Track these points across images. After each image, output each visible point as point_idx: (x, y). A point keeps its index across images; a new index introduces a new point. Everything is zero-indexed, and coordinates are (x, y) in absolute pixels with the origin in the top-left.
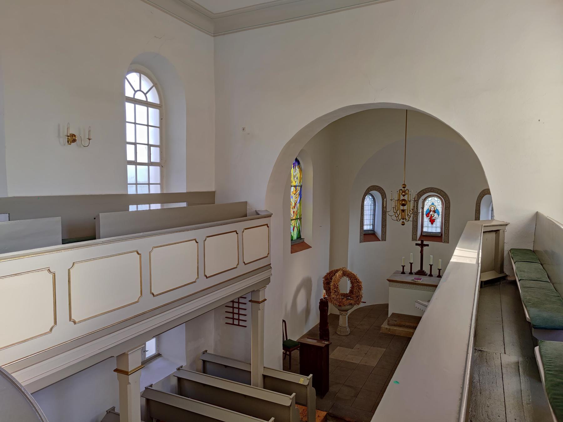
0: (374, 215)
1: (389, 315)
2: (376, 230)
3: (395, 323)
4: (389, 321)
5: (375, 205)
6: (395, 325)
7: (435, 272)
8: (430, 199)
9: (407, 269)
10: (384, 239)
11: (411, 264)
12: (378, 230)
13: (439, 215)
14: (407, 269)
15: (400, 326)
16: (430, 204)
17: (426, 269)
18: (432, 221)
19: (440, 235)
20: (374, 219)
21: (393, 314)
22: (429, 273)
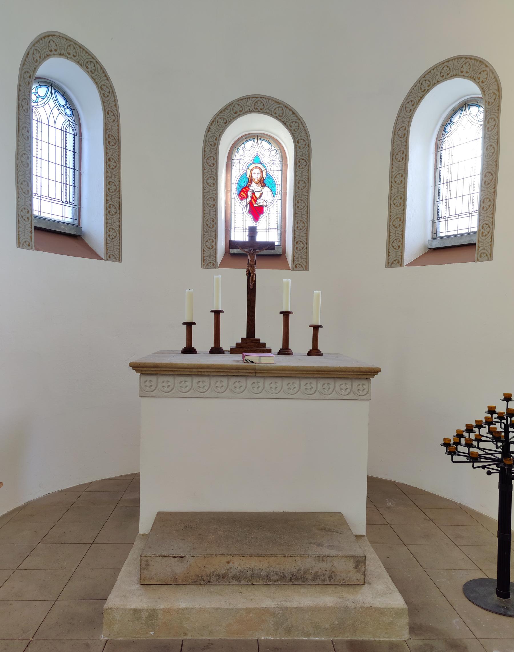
0: (78, 170)
1: (146, 521)
2: (85, 224)
3: (180, 569)
4: (145, 565)
5: (79, 134)
6: (176, 582)
7: (301, 342)
8: (249, 144)
9: (203, 340)
10: (113, 252)
11: (217, 313)
12: (94, 225)
13: (274, 193)
14: (203, 340)
15: (203, 580)
16: (248, 159)
17: (269, 332)
18: (256, 212)
19: (278, 251)
20: (78, 186)
21: (163, 519)
22: (276, 345)
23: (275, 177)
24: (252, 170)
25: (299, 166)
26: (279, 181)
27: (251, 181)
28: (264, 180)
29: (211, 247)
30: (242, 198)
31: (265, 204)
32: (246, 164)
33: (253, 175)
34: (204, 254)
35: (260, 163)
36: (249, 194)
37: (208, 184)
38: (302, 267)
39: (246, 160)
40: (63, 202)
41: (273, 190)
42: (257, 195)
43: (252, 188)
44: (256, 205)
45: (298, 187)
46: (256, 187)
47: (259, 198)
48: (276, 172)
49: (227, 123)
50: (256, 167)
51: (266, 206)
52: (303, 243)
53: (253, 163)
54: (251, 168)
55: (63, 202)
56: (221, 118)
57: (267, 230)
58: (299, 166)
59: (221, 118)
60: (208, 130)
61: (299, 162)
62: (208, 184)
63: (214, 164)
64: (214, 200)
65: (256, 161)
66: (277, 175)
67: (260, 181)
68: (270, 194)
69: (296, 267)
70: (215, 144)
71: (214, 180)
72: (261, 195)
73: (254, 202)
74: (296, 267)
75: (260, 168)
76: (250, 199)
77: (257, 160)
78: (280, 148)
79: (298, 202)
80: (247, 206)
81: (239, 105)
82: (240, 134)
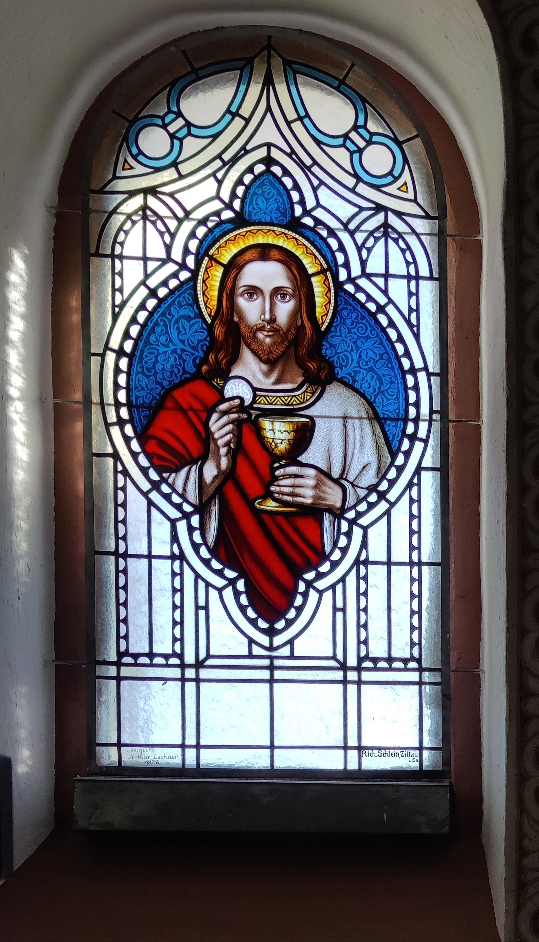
13: (391, 428)
16: (202, 195)
24: (233, 268)
26: (424, 348)
27: (228, 336)
28: (320, 336)
31: (333, 496)
32: (187, 227)
33: (242, 302)
35: (294, 225)
36: (220, 428)
39: (189, 199)
40: (343, 667)
42: (278, 433)
44: (271, 505)
46: (267, 383)
48: (398, 290)
51: (338, 514)
53: (241, 221)
55: (343, 667)
65: (262, 207)
66: (399, 282)
72: (303, 436)
73: (252, 486)
75: (289, 260)
76: (224, 463)
77: (267, 203)
78: (422, 133)
80: (202, 509)
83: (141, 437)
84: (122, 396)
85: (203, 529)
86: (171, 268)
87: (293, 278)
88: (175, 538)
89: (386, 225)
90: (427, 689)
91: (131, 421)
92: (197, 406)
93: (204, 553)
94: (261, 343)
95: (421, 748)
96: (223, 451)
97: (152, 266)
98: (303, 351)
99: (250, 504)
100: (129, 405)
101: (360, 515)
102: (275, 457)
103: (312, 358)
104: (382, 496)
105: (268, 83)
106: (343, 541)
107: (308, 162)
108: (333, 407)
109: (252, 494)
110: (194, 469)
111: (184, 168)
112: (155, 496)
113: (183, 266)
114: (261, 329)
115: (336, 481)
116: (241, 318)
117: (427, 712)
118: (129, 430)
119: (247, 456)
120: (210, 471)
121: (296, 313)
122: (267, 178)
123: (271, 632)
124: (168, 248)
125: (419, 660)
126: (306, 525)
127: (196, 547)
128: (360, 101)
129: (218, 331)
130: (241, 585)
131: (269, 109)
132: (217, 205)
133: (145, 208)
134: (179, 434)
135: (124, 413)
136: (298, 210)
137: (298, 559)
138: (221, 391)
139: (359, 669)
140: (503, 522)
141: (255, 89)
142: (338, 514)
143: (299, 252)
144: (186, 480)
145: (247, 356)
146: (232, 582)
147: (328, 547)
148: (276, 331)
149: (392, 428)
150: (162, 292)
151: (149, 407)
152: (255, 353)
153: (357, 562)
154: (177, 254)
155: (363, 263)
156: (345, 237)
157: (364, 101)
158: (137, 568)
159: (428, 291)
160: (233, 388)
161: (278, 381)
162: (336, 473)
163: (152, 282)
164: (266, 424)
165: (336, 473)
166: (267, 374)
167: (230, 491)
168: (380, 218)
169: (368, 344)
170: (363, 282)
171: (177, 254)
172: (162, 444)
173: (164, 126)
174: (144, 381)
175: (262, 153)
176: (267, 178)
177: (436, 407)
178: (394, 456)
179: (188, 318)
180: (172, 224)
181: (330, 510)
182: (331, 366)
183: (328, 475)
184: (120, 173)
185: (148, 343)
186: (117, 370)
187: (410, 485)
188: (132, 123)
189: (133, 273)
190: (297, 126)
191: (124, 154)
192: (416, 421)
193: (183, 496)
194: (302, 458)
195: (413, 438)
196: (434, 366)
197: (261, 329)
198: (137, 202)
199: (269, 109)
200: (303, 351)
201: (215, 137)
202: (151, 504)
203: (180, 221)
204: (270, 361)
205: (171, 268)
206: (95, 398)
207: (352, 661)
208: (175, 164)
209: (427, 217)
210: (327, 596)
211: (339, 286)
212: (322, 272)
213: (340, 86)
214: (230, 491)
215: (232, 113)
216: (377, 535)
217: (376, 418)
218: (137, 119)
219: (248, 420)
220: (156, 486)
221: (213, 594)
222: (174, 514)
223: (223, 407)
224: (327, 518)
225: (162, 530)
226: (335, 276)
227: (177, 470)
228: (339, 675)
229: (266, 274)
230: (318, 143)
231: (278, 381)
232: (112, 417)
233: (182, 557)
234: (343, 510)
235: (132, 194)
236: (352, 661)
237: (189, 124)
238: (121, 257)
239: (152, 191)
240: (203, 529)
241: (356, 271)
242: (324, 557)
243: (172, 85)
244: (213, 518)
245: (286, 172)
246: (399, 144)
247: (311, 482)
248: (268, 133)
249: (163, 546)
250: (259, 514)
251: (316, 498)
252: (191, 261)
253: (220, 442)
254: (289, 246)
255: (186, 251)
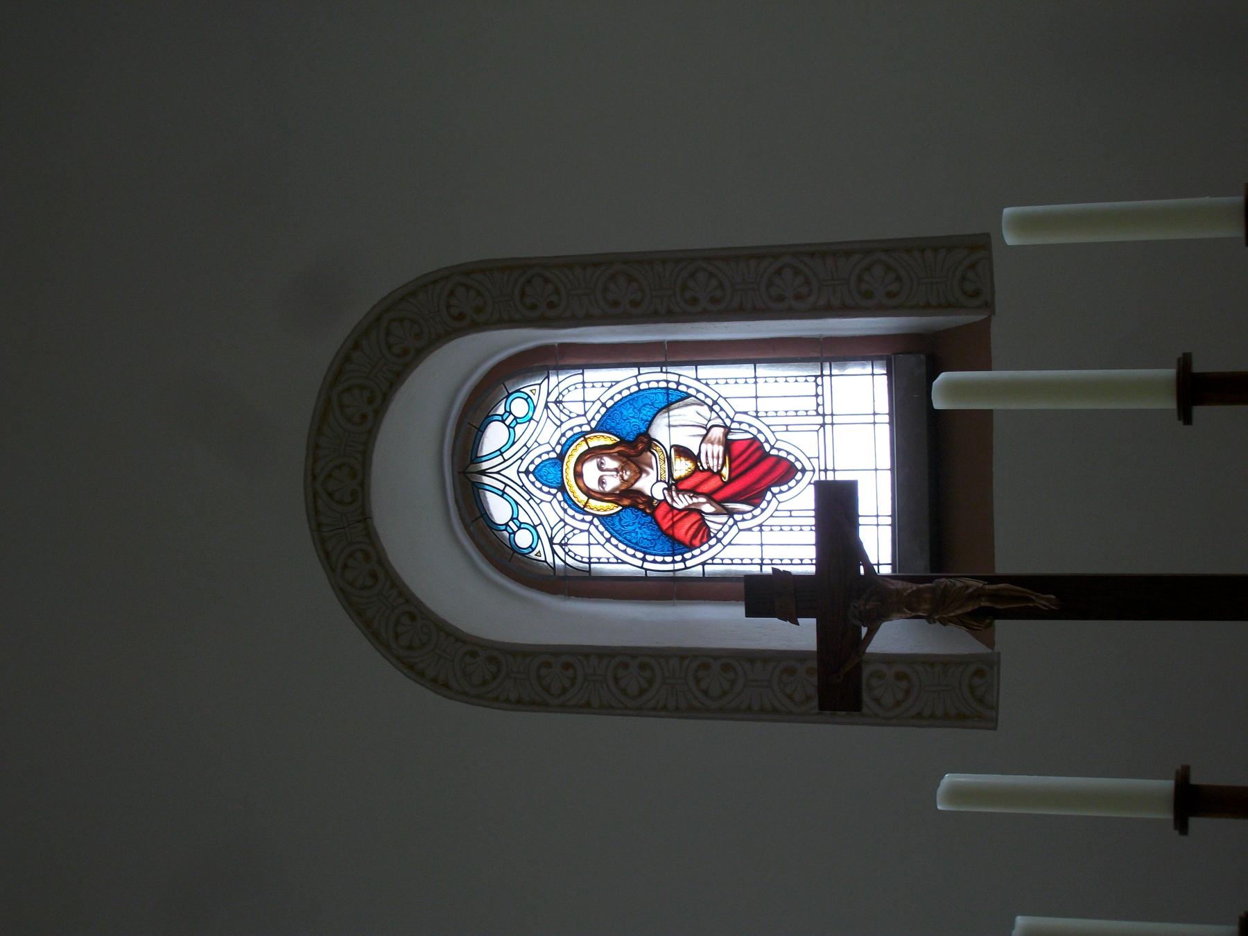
13: (672, 399)
16: (550, 511)
18: (752, 471)
23: (610, 396)
24: (589, 493)
25: (551, 305)
29: (904, 684)
30: (703, 533)
31: (717, 433)
33: (608, 488)
34: (932, 716)
35: (561, 457)
36: (682, 502)
37: (642, 692)
38: (972, 266)
39: (553, 519)
40: (823, 425)
41: (661, 400)
42: (682, 467)
43: (658, 493)
44: (725, 472)
45: (635, 304)
46: (653, 473)
47: (695, 458)
48: (592, 394)
49: (411, 611)
50: (578, 475)
51: (728, 430)
52: (868, 268)
53: (562, 488)
54: (581, 498)
55: (823, 425)
56: (397, 636)
57: (825, 420)
58: (551, 305)
59: (397, 636)
60: (441, 686)
61: (534, 307)
62: (642, 692)
63: (567, 666)
64: (706, 666)
67: (628, 457)
68: (681, 414)
69: (976, 294)
70: (491, 659)
71: (626, 666)
72: (683, 452)
73: (714, 483)
74: (976, 294)
75: (582, 460)
76: (702, 500)
79: (695, 301)
80: (731, 513)
81: (345, 566)
82: (457, 540)
83: (691, 548)
84: (669, 559)
85: (743, 513)
86: (592, 529)
87: (591, 458)
88: (750, 529)
89: (557, 402)
90: (834, 372)
91: (682, 554)
92: (670, 516)
93: (757, 512)
94: (630, 477)
95: (873, 374)
96: (695, 500)
97: (593, 541)
98: (632, 452)
99: (725, 484)
100: (673, 555)
101: (728, 416)
102: (696, 469)
103: (636, 447)
104: (715, 403)
105: (484, 473)
106: (744, 427)
107: (525, 449)
108: (660, 431)
109: (720, 483)
110: (707, 517)
111: (537, 522)
112: (725, 541)
113: (591, 523)
114: (622, 477)
115: (708, 431)
116: (617, 489)
117: (846, 372)
118: (687, 556)
119: (697, 486)
120: (708, 508)
121: (611, 456)
122: (537, 473)
123: (804, 471)
124: (582, 531)
125: (816, 377)
126: (736, 450)
127: (754, 517)
128: (487, 420)
129: (626, 502)
130: (775, 490)
131: (498, 473)
132: (555, 502)
133: (560, 544)
134: (687, 526)
135: (678, 558)
136: (553, 455)
137: (758, 454)
138: (660, 502)
139: (824, 415)
140: (726, 324)
141: (486, 480)
142: (728, 430)
143: (576, 455)
144: (715, 523)
145: (638, 485)
146: (774, 495)
147: (749, 436)
148: (622, 469)
149: (673, 398)
150: (607, 535)
151: (673, 543)
152: (636, 481)
153: (757, 417)
154: (585, 526)
155: (578, 416)
156: (565, 427)
157: (488, 416)
158: (769, 553)
159: (590, 375)
160: (658, 495)
161: (651, 467)
162: (704, 432)
163: (602, 541)
164: (676, 475)
165: (704, 432)
166: (648, 473)
167: (719, 496)
168: (552, 406)
169: (625, 413)
170: (589, 416)
171: (585, 526)
172: (694, 536)
173: (514, 533)
174: (659, 546)
175: (523, 476)
176: (537, 473)
177: (658, 369)
178: (689, 396)
179: (620, 520)
180: (568, 529)
181: (726, 435)
182: (640, 435)
183: (705, 436)
184: (542, 558)
185: (637, 544)
186: (654, 562)
187: (707, 384)
188: (515, 551)
189: (597, 552)
190: (506, 455)
191: (533, 555)
192: (668, 382)
193: (724, 524)
194: (696, 453)
195: (678, 383)
196: (634, 371)
197: (622, 477)
198: (557, 548)
199: (498, 473)
200: (632, 452)
201: (517, 504)
202: (730, 544)
203: (566, 524)
204: (640, 472)
205: (592, 529)
206: (671, 574)
207: (819, 420)
208: (535, 527)
209: (548, 377)
210: (778, 435)
211: (593, 431)
212: (586, 440)
213: (481, 430)
214: (719, 496)
215: (503, 494)
216: (740, 405)
217: (668, 407)
218: (512, 548)
219: (675, 485)
220: (719, 541)
221: (781, 507)
222: (735, 529)
223: (669, 500)
224: (730, 437)
225: (744, 537)
226: (588, 433)
227: (708, 528)
228: (828, 428)
229: (591, 472)
230: (514, 443)
231: (651, 467)
232: (681, 566)
233: (761, 525)
234: (725, 427)
235: (554, 552)
236: (819, 420)
237: (512, 519)
238: (590, 558)
239: (551, 540)
240: (743, 513)
241: (583, 420)
242: (755, 439)
243: (491, 528)
244: (928, 319)
245: (532, 462)
246: (509, 395)
247: (710, 445)
248: (511, 472)
249: (754, 537)
250: (731, 480)
251: (719, 443)
252: (589, 518)
253: (690, 502)
254: (573, 460)
255: (583, 520)
